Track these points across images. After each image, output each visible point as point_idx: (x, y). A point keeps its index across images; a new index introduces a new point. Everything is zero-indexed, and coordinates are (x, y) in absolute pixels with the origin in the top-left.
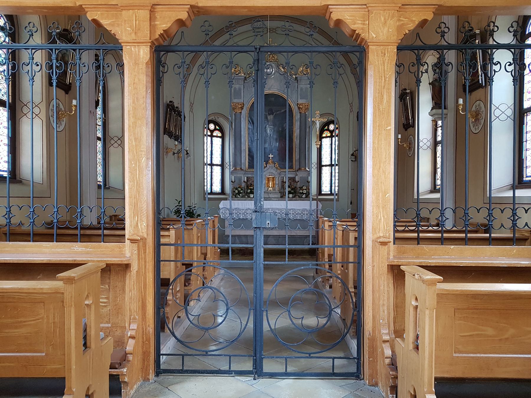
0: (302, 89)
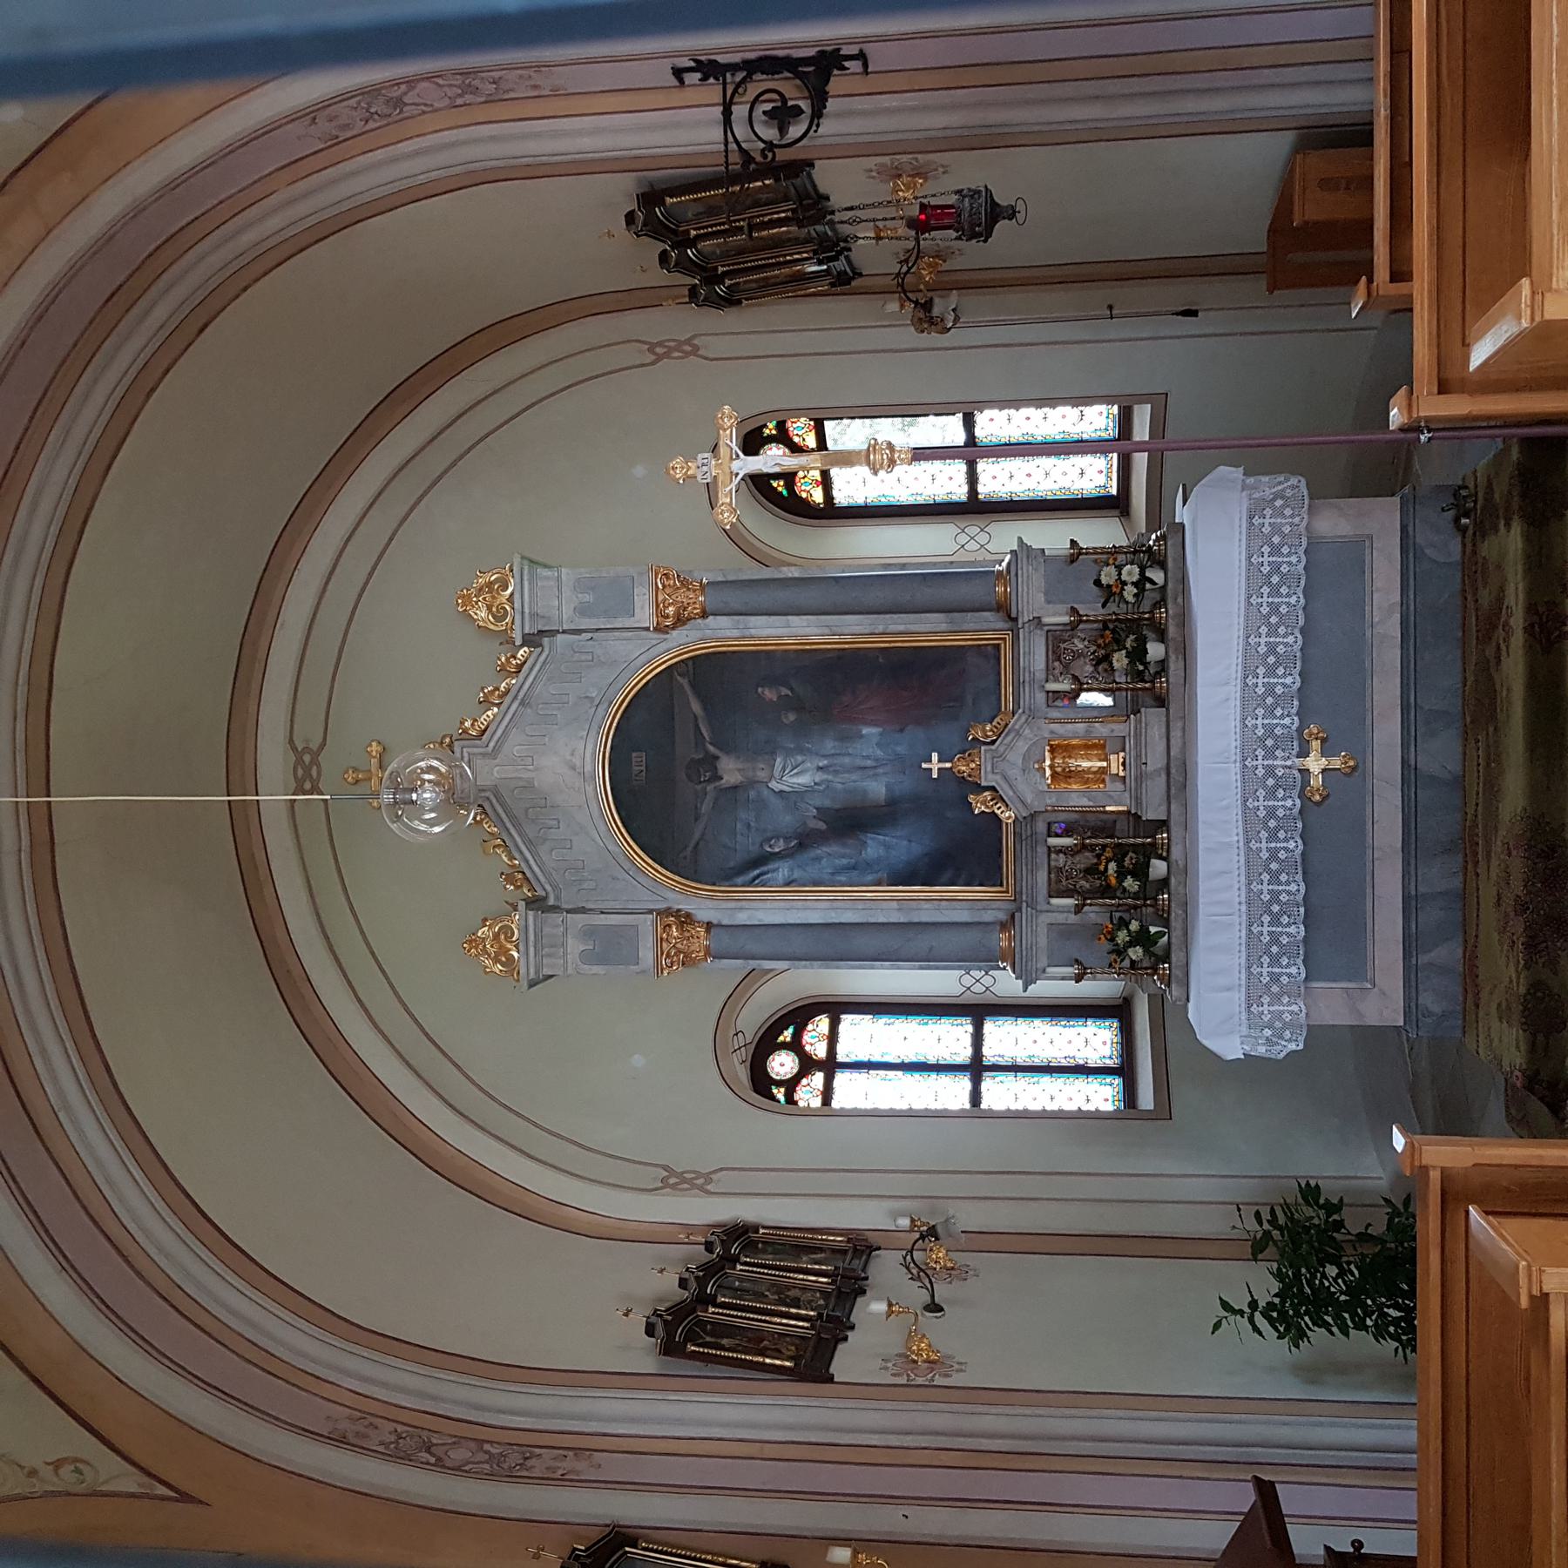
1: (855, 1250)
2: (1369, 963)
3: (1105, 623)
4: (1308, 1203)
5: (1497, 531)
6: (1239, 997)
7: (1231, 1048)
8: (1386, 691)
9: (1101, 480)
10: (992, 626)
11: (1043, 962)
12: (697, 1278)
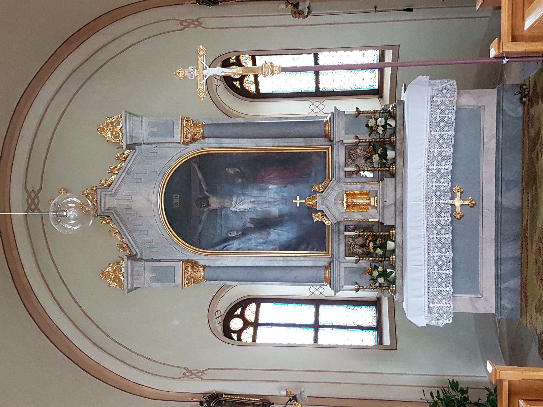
0: (152, 135)
1: (263, 405)
2: (480, 287)
3: (370, 143)
4: (453, 390)
5: (538, 103)
6: (424, 300)
7: (421, 321)
8: (489, 171)
9: (371, 82)
10: (323, 144)
11: (342, 283)
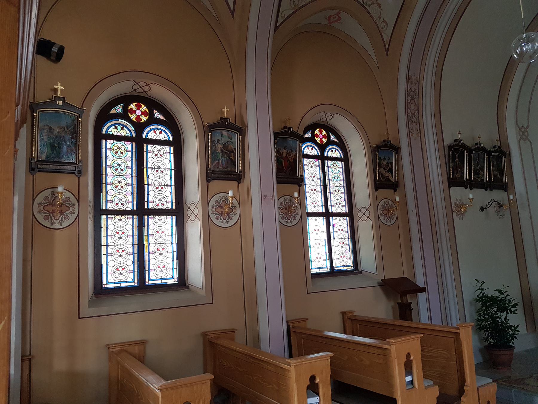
9: (111, 278)
12: (479, 147)
